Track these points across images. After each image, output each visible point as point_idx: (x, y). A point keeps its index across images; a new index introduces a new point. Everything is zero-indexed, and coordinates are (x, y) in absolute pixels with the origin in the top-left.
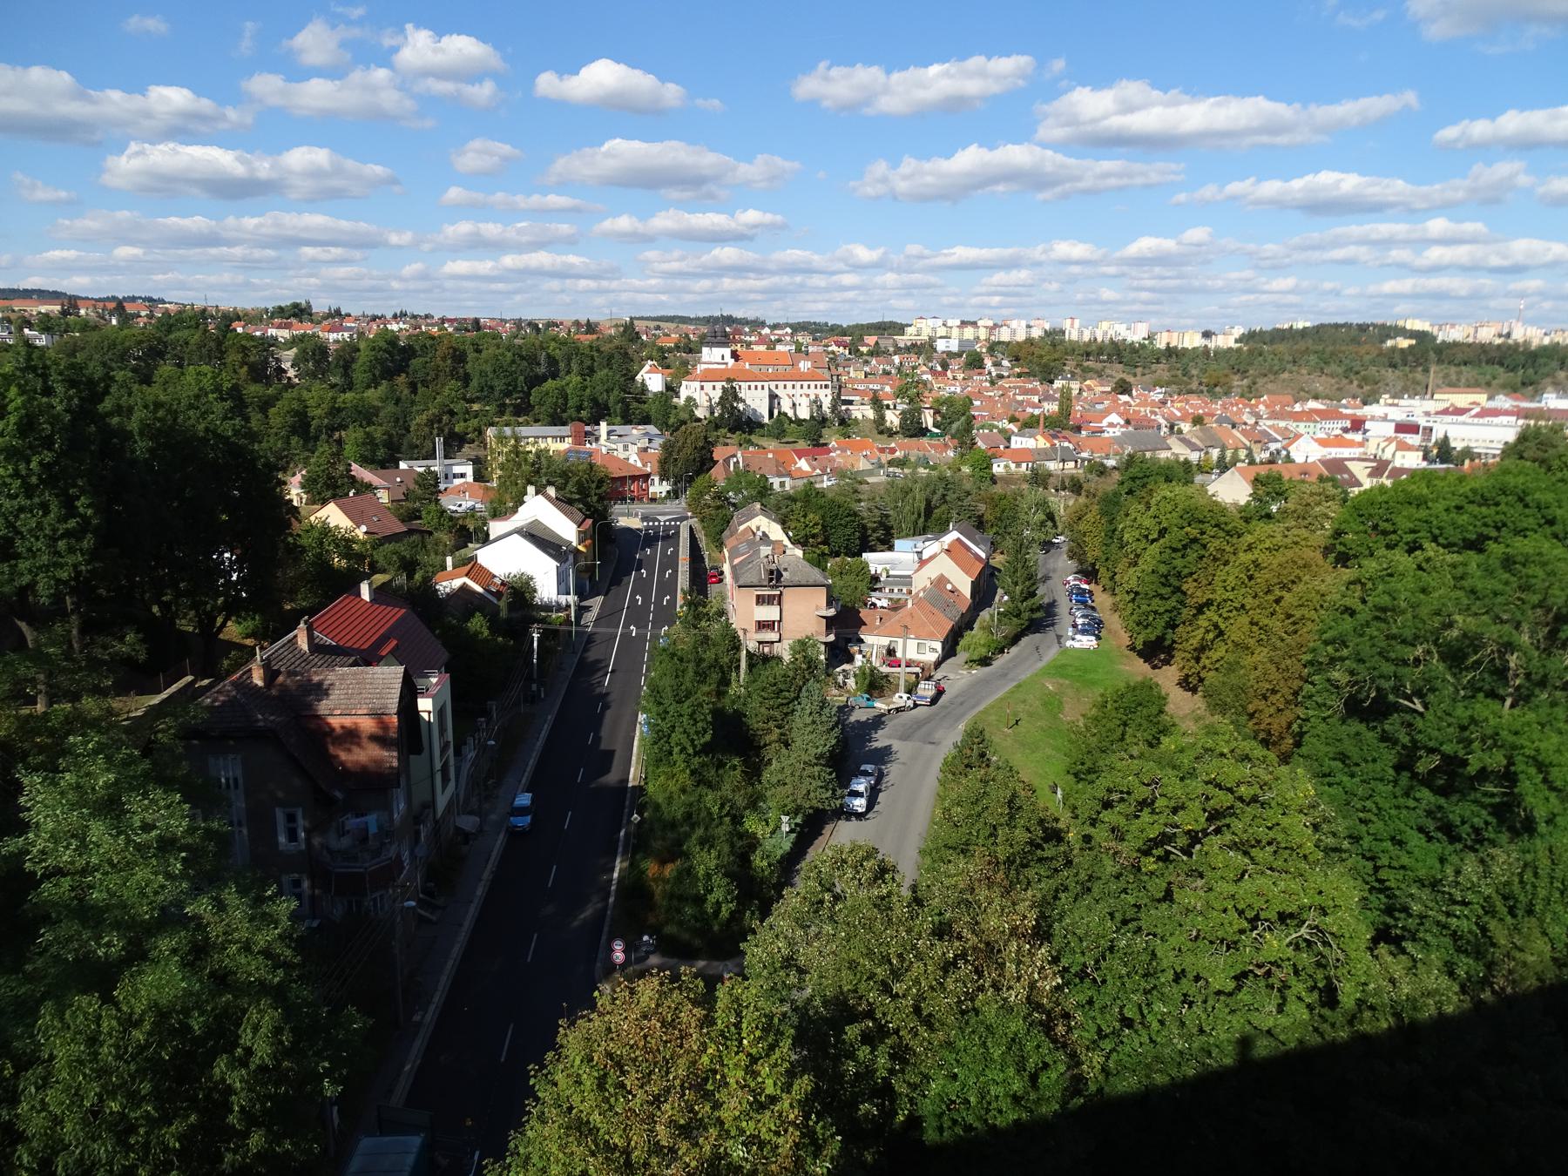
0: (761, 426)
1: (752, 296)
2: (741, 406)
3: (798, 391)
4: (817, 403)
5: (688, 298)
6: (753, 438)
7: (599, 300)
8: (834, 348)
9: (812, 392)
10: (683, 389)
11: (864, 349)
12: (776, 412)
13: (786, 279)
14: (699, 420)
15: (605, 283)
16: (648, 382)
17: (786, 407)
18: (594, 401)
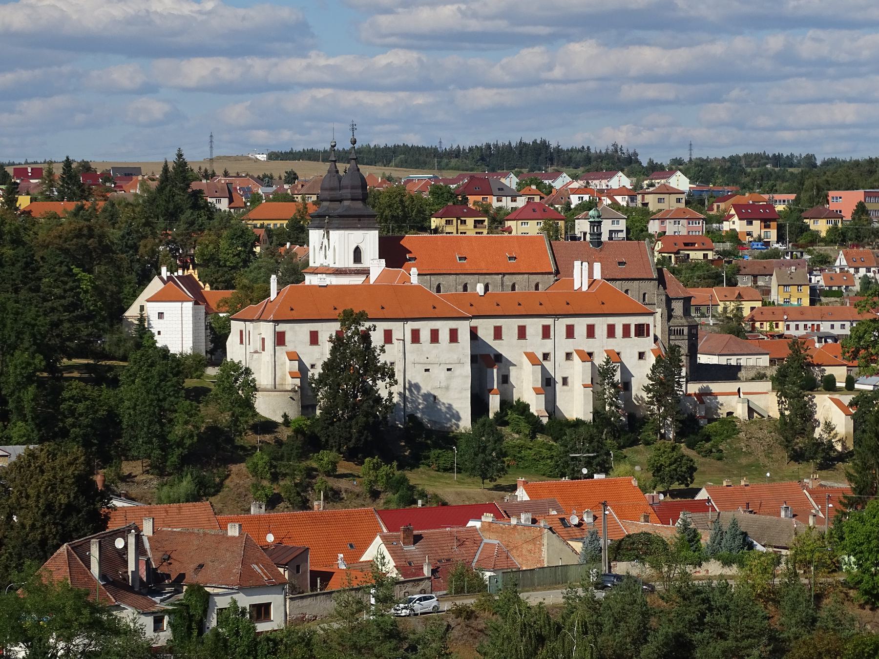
0: (445, 438)
3: (561, 344)
6: (416, 478)
7: (237, 111)
8: (737, 225)
9: (600, 347)
11: (821, 227)
12: (494, 403)
13: (742, 43)
14: (268, 426)
15: (258, 66)
16: (156, 326)
17: (525, 387)
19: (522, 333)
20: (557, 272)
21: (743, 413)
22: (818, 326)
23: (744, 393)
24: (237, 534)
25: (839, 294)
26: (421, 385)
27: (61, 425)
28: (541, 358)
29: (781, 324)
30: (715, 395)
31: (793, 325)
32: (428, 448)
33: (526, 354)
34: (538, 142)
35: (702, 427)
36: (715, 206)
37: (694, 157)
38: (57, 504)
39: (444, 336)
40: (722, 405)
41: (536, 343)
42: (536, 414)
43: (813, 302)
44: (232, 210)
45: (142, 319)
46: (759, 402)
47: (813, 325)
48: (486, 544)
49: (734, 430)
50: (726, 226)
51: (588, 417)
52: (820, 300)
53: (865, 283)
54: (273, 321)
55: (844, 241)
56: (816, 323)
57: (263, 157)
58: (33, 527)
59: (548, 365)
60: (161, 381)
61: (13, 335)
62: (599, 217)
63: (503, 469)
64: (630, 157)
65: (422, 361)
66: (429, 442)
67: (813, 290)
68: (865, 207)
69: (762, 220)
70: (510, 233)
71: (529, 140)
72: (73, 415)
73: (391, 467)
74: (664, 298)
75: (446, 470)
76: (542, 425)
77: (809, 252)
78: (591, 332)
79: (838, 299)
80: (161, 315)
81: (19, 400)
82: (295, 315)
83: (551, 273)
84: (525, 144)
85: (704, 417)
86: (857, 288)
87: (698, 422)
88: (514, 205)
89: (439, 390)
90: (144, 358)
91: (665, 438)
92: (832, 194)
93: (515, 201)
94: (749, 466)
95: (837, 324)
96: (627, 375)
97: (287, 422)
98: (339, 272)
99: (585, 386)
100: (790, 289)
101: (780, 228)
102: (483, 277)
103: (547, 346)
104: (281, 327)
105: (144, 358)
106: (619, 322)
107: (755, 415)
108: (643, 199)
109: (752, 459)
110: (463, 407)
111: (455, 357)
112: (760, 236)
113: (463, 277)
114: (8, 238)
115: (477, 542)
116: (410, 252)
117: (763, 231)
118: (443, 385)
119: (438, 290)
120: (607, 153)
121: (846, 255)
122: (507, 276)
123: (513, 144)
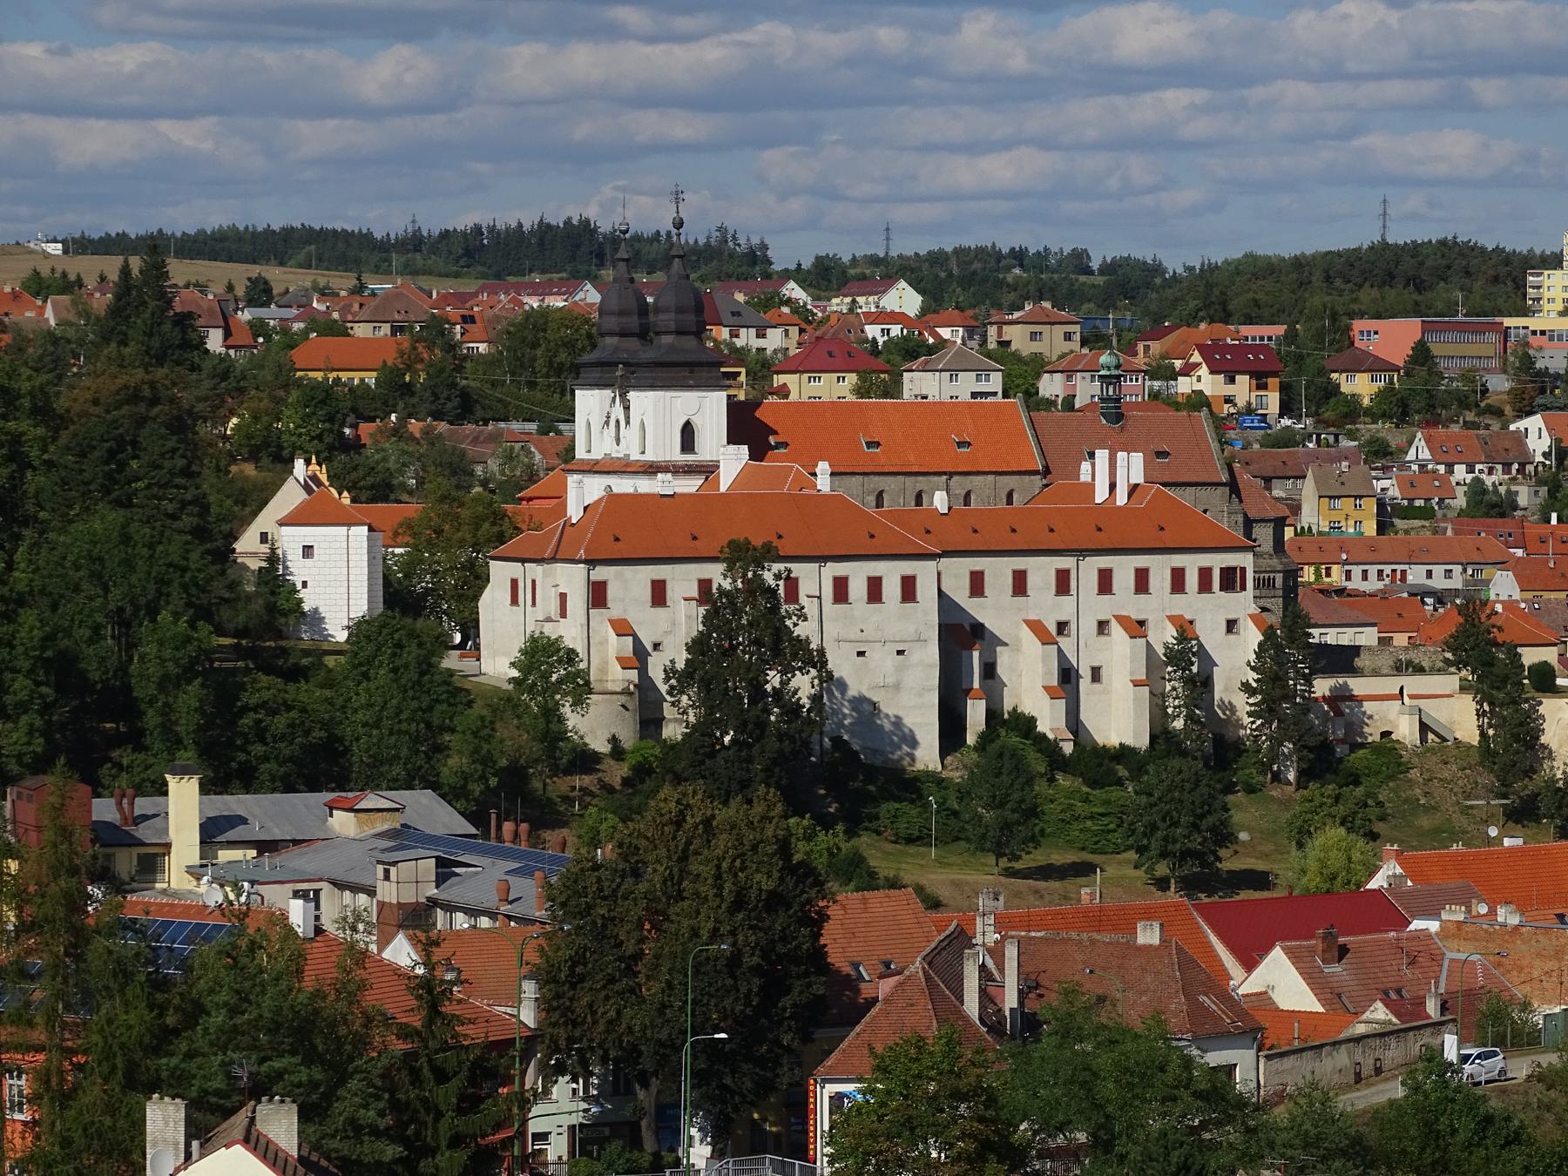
0: (909, 786)
1: (648, 125)
2: (804, 685)
3: (1088, 605)
4: (1186, 662)
5: (316, 137)
8: (1207, 383)
9: (1159, 607)
10: (493, 605)
11: (1361, 386)
12: (976, 713)
14: (585, 760)
16: (298, 571)
17: (1027, 684)
18: (62, 669)
19: (1020, 584)
20: (1047, 471)
21: (1411, 734)
22: (1404, 572)
23: (1411, 697)
24: (1156, 941)
25: (1426, 513)
26: (848, 682)
27: (242, 757)
28: (1053, 629)
29: (1335, 568)
30: (1359, 700)
31: (1357, 571)
32: (874, 800)
33: (1028, 623)
34: (575, 222)
35: (1341, 760)
36: (1140, 347)
37: (894, 253)
38: (753, 894)
39: (891, 589)
40: (1370, 717)
41: (1044, 603)
42: (1051, 736)
43: (1382, 528)
44: (232, 352)
45: (273, 559)
46: (1438, 713)
47: (1394, 571)
48: (1452, 960)
49: (1399, 765)
50: (1184, 385)
51: (1143, 742)
52: (1392, 524)
53: (1476, 493)
54: (586, 562)
55: (1405, 414)
56: (1399, 568)
57: (55, 249)
58: (715, 935)
59: (1066, 644)
60: (422, 674)
61: (152, 587)
62: (1118, 367)
63: (1033, 839)
64: (752, 252)
65: (852, 637)
66: (872, 788)
67: (1381, 505)
68: (1428, 350)
69: (1252, 374)
70: (787, 396)
71: (557, 220)
72: (264, 742)
73: (835, 835)
74: (1240, 519)
75: (910, 840)
76: (1064, 756)
77: (1351, 435)
78: (1142, 582)
79: (1427, 523)
80: (308, 551)
81: (167, 709)
82: (622, 550)
83: (1036, 473)
84: (549, 225)
85: (1342, 741)
86: (1461, 501)
87: (1333, 751)
88: (761, 343)
89: (883, 691)
90: (385, 632)
91: (1279, 781)
92: (1358, 325)
93: (764, 336)
94: (1438, 830)
95: (1438, 570)
96: (1208, 662)
97: (617, 752)
98: (651, 469)
99: (1136, 684)
100: (1338, 503)
101: (1284, 389)
102: (912, 478)
103: (1065, 608)
104: (600, 573)
105: (385, 632)
106: (1192, 564)
107: (1431, 736)
108: (1000, 334)
109: (1438, 819)
110: (924, 723)
111: (909, 629)
112: (1249, 403)
113: (877, 478)
114: (26, 403)
115: (1436, 958)
116: (775, 433)
117: (1253, 395)
118: (890, 680)
119: (879, 502)
120: (708, 244)
121: (1428, 441)
122: (955, 478)
123: (527, 227)
